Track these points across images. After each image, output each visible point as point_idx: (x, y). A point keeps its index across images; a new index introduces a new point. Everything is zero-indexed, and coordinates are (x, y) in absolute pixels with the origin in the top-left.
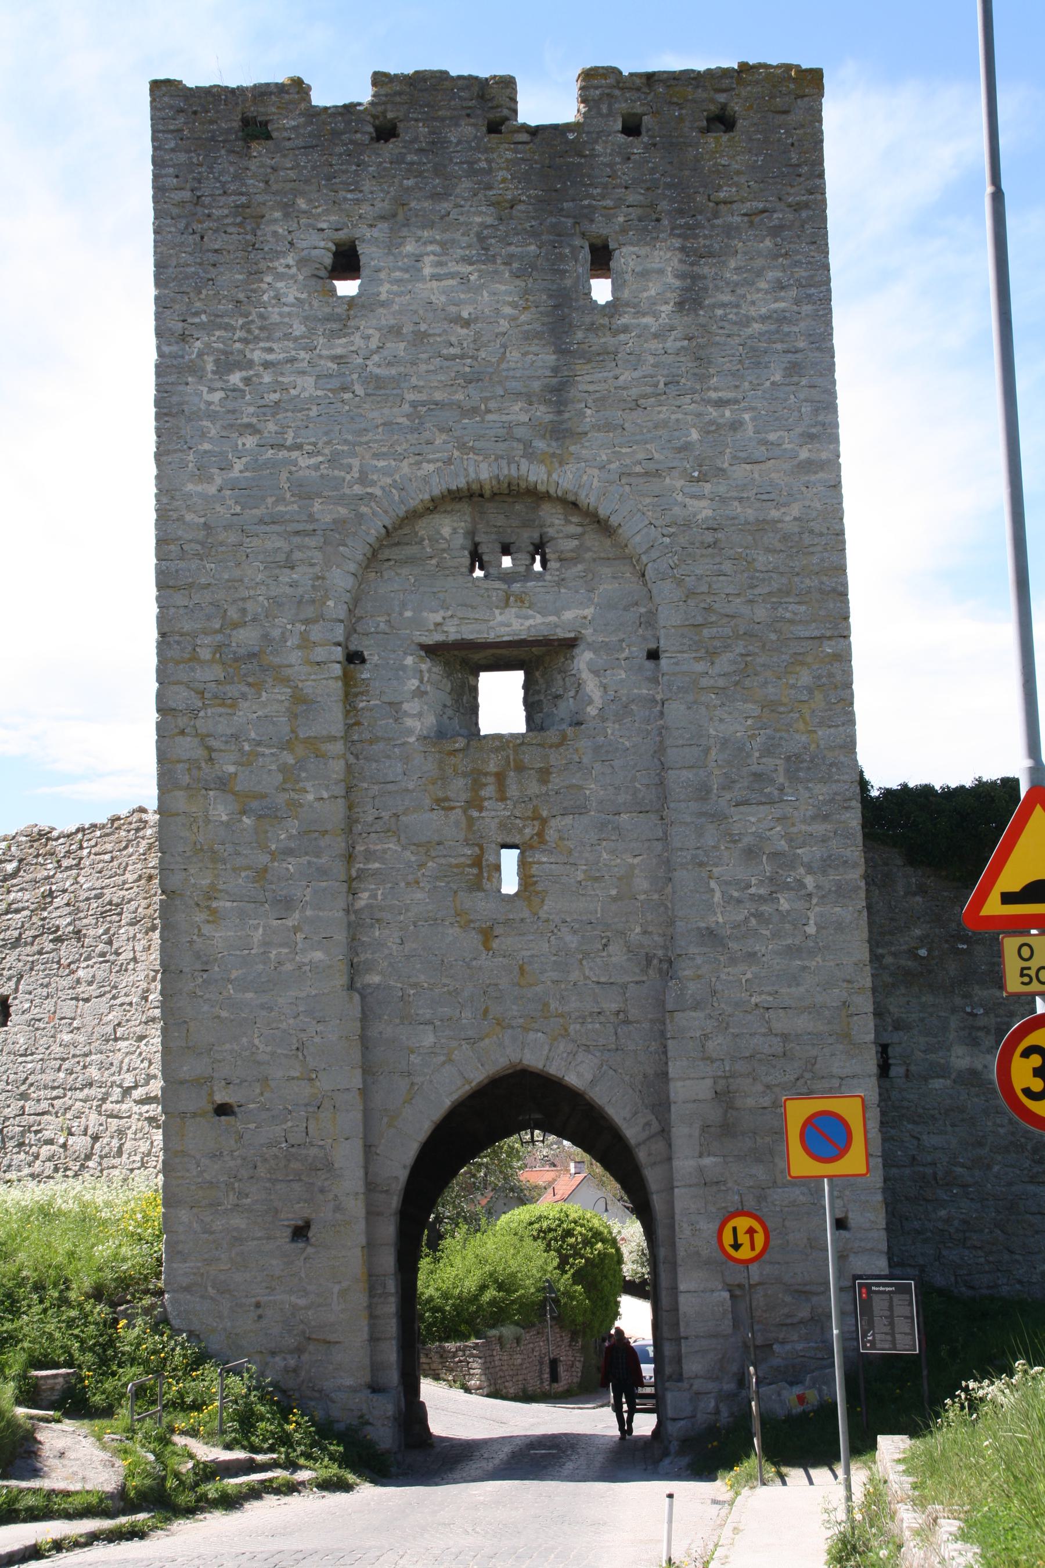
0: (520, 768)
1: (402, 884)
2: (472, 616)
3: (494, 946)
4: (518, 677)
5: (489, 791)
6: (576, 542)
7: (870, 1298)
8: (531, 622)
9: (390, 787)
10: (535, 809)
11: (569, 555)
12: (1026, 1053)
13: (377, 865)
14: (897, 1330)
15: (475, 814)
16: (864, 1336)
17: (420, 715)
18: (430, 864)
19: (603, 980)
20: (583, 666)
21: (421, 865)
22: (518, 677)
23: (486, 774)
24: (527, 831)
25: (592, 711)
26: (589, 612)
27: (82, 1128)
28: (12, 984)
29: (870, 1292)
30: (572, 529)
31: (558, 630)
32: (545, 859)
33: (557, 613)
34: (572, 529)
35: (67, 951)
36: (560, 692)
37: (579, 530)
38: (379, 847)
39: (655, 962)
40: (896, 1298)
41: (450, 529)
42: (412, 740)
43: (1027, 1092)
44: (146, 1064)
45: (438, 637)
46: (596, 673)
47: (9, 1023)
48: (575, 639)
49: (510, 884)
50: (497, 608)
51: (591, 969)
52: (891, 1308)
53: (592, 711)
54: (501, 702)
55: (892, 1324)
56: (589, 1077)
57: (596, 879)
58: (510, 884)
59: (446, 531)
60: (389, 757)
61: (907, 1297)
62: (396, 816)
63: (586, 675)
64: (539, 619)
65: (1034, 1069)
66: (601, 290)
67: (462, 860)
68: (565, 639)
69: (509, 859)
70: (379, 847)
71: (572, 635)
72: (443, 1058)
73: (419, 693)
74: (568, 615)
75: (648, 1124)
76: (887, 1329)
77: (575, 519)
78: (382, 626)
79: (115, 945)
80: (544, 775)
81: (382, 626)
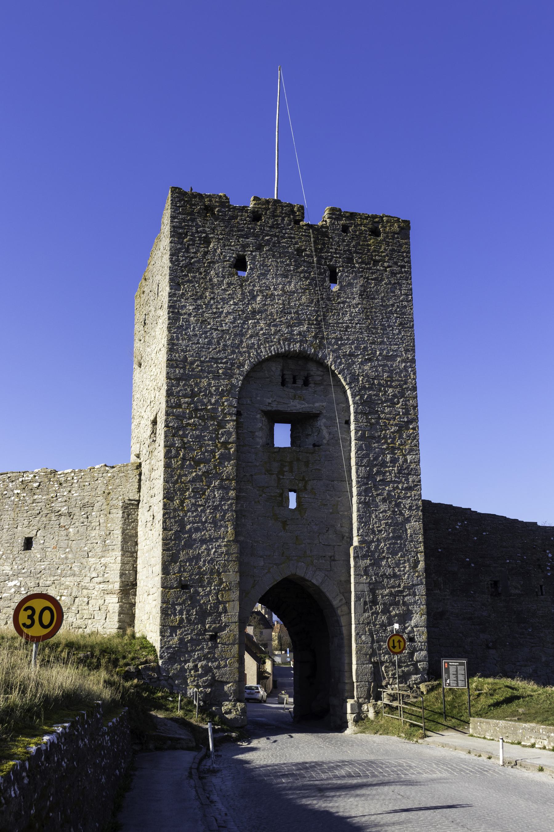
0: (298, 460)
1: (253, 502)
2: (282, 401)
3: (287, 528)
4: (289, 426)
5: (286, 469)
6: (321, 378)
7: (448, 668)
8: (303, 406)
9: (250, 464)
10: (303, 477)
11: (318, 382)
12: (26, 610)
13: (244, 494)
14: (459, 679)
15: (281, 477)
16: (446, 681)
17: (261, 438)
18: (264, 495)
19: (326, 544)
20: (322, 424)
21: (260, 496)
22: (289, 426)
23: (116, 655)
24: (300, 485)
25: (325, 441)
26: (324, 404)
27: (69, 593)
28: (34, 532)
29: (448, 665)
30: (319, 373)
31: (313, 410)
32: (306, 496)
33: (313, 403)
34: (319, 373)
35: (63, 521)
36: (310, 433)
37: (322, 373)
38: (244, 487)
39: (345, 538)
40: (459, 667)
41: (276, 369)
42: (258, 447)
43: (24, 625)
44: (103, 568)
45: (269, 408)
46: (327, 427)
47: (32, 549)
48: (319, 414)
49: (293, 504)
50: (291, 399)
51: (322, 539)
52: (457, 671)
53: (325, 441)
54: (282, 436)
55: (457, 677)
56: (320, 581)
57: (325, 505)
58: (293, 504)
59: (274, 369)
60: (250, 453)
61: (463, 667)
62: (252, 475)
63: (323, 428)
64: (307, 405)
65: (28, 616)
66: (335, 288)
67: (276, 494)
68: (315, 413)
69: (293, 496)
70: (244, 487)
71: (318, 412)
72: (266, 571)
73: (261, 429)
74: (317, 405)
75: (341, 600)
76: (455, 679)
77: (320, 369)
78: (248, 401)
79: (90, 519)
80: (307, 464)
81: (248, 401)
